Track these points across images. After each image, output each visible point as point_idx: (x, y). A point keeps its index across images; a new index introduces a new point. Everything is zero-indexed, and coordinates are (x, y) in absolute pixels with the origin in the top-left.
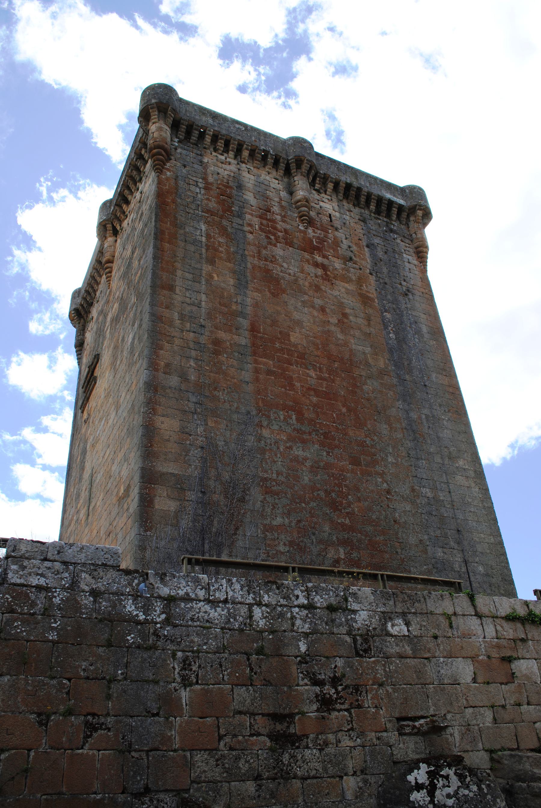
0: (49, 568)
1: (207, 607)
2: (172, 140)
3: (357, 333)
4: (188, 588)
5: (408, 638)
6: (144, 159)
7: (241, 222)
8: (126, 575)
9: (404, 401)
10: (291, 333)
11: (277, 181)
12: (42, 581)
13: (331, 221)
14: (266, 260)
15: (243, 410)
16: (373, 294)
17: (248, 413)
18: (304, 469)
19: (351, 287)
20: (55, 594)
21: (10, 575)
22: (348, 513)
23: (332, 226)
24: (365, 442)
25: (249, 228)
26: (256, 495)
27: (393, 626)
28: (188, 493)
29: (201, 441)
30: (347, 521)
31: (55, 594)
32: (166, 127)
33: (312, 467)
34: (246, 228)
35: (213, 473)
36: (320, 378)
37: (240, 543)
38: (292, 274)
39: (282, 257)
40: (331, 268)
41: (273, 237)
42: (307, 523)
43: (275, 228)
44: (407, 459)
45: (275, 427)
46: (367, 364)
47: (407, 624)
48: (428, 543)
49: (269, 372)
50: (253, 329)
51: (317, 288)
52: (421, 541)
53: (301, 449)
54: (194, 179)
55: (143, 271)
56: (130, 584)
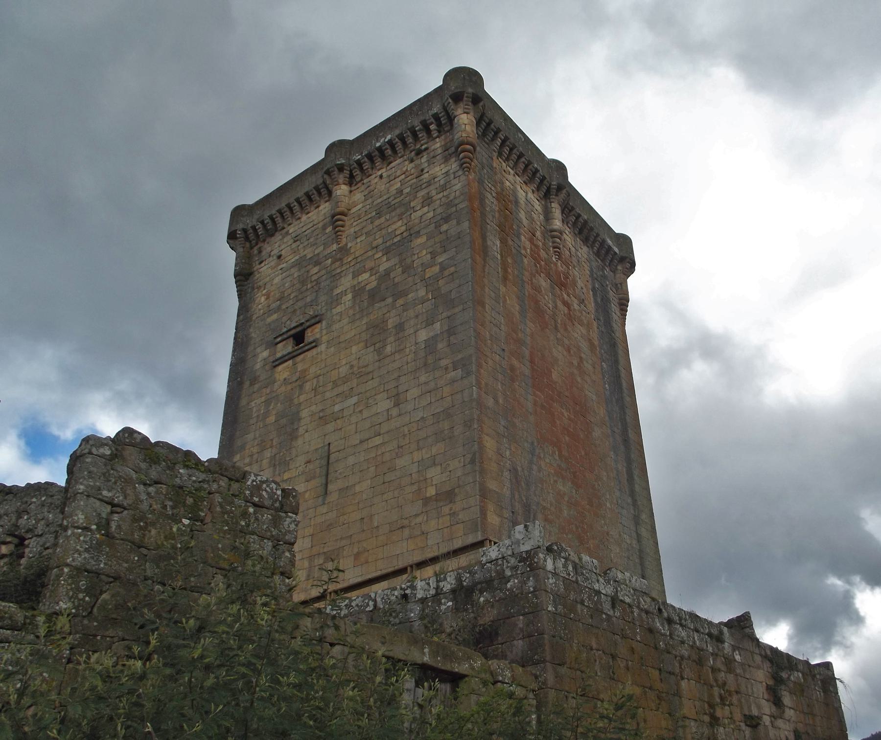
1: (681, 629)
16: (596, 343)
17: (532, 443)
34: (523, 252)
35: (517, 496)
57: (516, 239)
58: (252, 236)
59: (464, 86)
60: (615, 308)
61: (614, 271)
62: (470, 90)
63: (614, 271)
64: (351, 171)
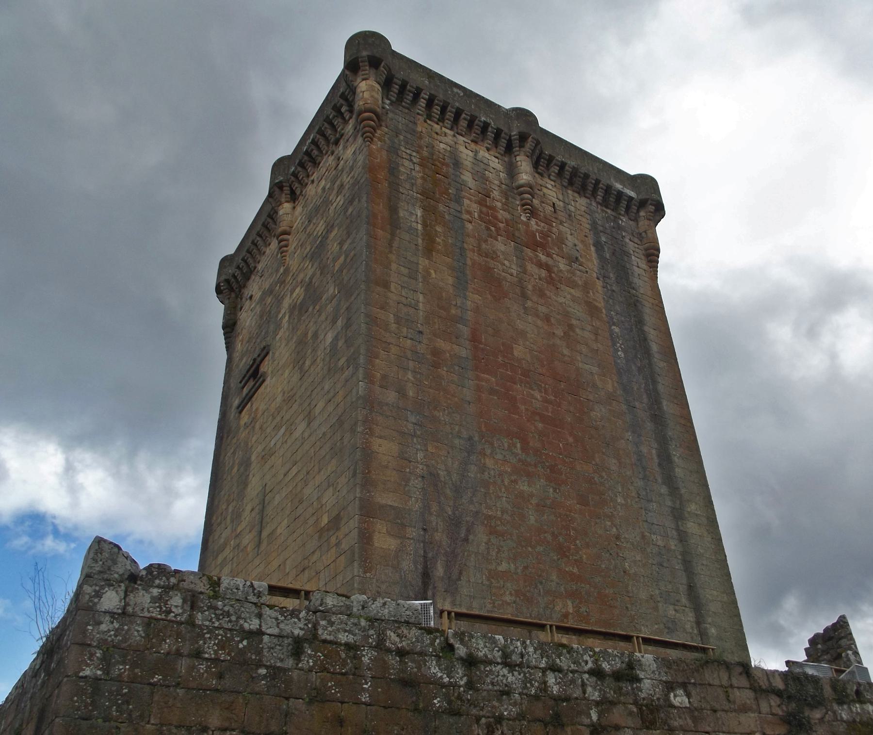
0: (356, 625)
1: (505, 671)
2: (383, 102)
3: (584, 350)
4: (486, 649)
5: (690, 710)
6: (344, 119)
7: (459, 209)
8: (428, 634)
9: (633, 432)
10: (514, 346)
11: (497, 160)
12: (351, 639)
13: (555, 212)
14: (487, 256)
15: (465, 434)
16: (601, 304)
17: (470, 439)
18: (530, 507)
19: (577, 293)
20: (364, 653)
21: (320, 632)
22: (575, 560)
23: (556, 218)
24: (593, 478)
25: (468, 216)
26: (481, 536)
27: (675, 696)
28: (409, 530)
29: (420, 469)
30: (575, 570)
31: (364, 653)
32: (377, 86)
33: (538, 505)
34: (466, 216)
35: (435, 508)
36: (546, 401)
37: (465, 591)
38: (515, 274)
39: (503, 253)
40: (555, 269)
41: (493, 229)
42: (533, 571)
43: (496, 218)
44: (637, 500)
45: (499, 456)
46: (594, 386)
47: (689, 695)
48: (659, 599)
49: (492, 392)
50: (474, 339)
51: (542, 294)
52: (652, 596)
53: (526, 484)
54: (408, 151)
55: (348, 260)
56: (432, 644)
57: (453, 205)
58: (235, 285)
59: (368, 54)
60: (637, 262)
61: (636, 220)
62: (365, 53)
63: (636, 220)
64: (290, 186)
